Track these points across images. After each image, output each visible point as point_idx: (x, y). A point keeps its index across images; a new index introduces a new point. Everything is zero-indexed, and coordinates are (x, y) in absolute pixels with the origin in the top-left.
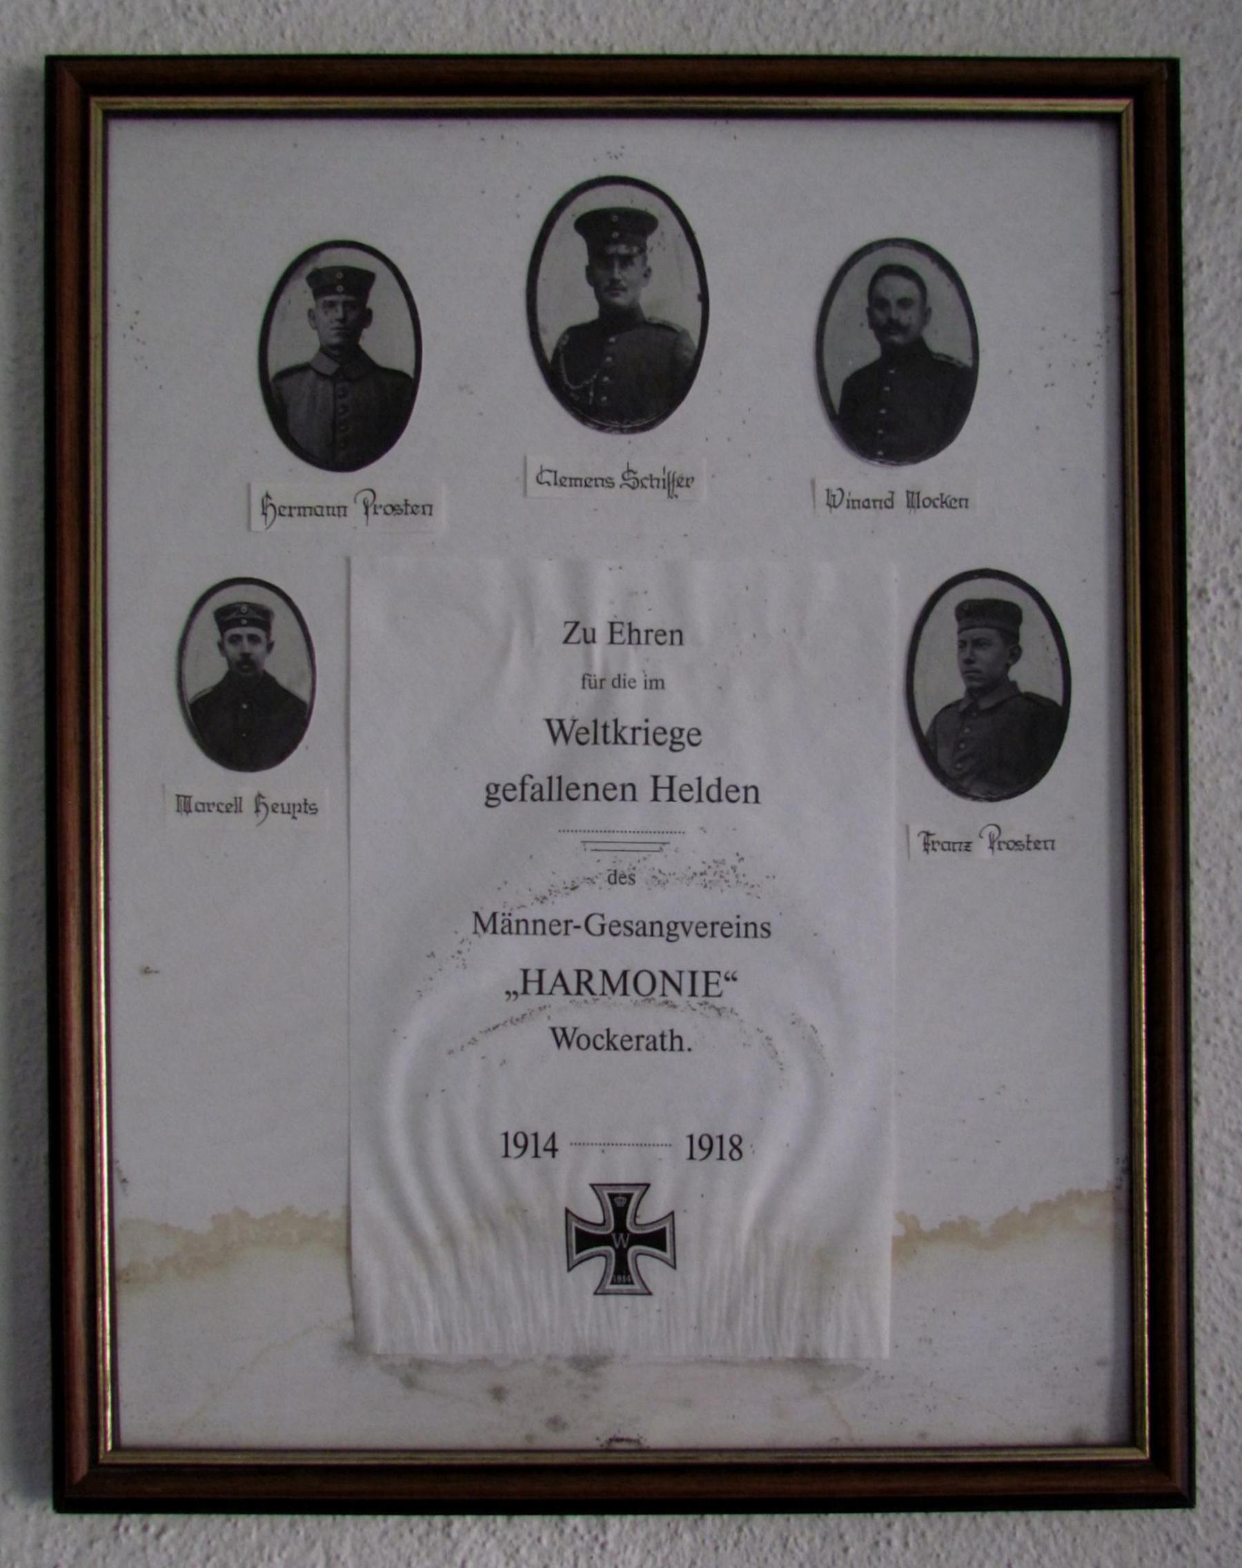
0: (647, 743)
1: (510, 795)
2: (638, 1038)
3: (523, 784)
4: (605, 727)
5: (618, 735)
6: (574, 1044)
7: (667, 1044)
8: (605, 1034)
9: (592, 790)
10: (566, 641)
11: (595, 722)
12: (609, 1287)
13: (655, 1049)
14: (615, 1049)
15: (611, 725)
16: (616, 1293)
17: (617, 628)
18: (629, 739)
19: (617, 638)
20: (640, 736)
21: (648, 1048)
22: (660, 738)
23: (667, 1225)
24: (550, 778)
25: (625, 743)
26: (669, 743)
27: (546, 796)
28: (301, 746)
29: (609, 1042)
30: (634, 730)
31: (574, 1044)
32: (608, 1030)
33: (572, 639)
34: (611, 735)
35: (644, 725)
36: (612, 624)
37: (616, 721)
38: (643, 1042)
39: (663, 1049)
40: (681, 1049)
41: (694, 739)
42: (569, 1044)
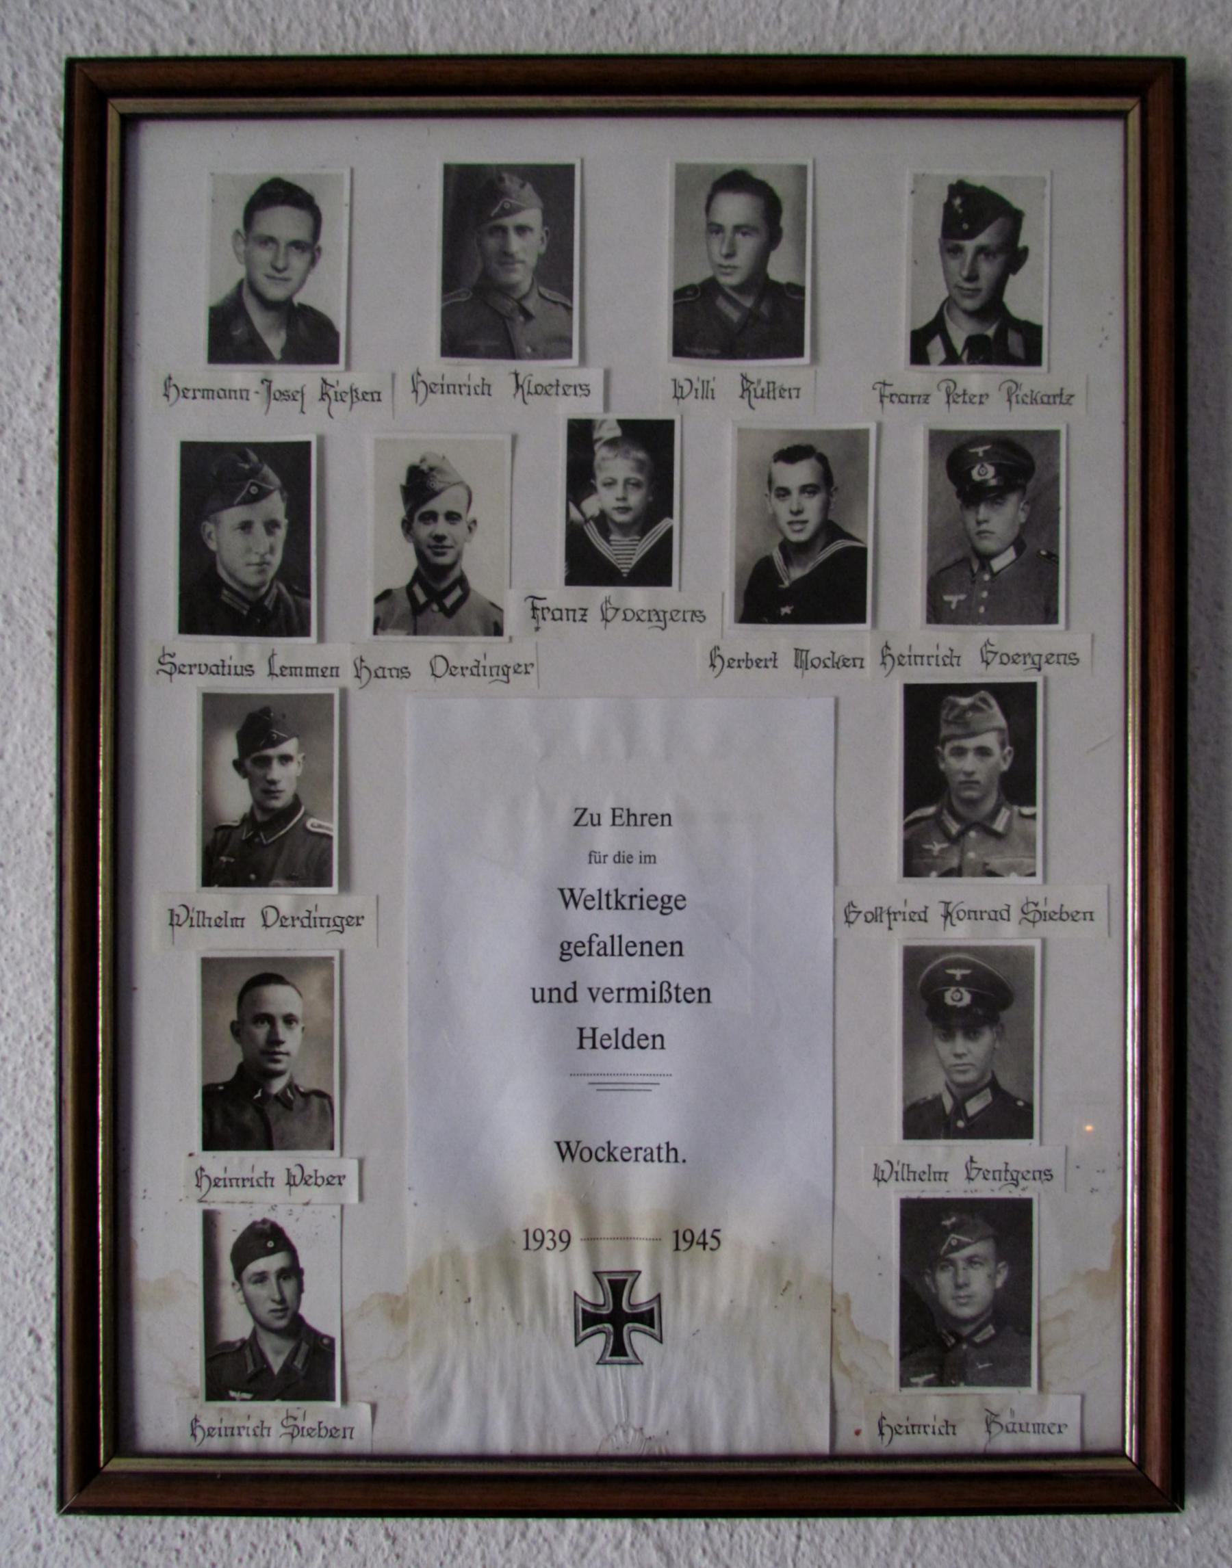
0: (642, 908)
1: (580, 951)
2: (637, 1150)
3: (590, 942)
4: (608, 895)
5: (618, 902)
6: (577, 1156)
7: (663, 1157)
8: (606, 1146)
9: (646, 947)
10: (576, 824)
11: (600, 890)
12: (608, 1358)
13: (652, 1160)
14: (616, 1160)
15: (613, 893)
16: (612, 1363)
17: (618, 812)
18: (627, 905)
19: (618, 821)
20: (636, 902)
21: (645, 1160)
22: (653, 904)
23: (655, 1305)
24: (612, 937)
25: (624, 908)
26: (659, 908)
27: (609, 951)
28: (1007, 196)
29: (610, 1154)
30: (631, 897)
31: (577, 1156)
32: (609, 1143)
33: (581, 822)
34: (612, 903)
35: (639, 894)
36: (614, 810)
37: (617, 890)
38: (641, 1154)
39: (660, 1161)
40: (676, 1161)
41: (680, 904)
42: (573, 1157)
